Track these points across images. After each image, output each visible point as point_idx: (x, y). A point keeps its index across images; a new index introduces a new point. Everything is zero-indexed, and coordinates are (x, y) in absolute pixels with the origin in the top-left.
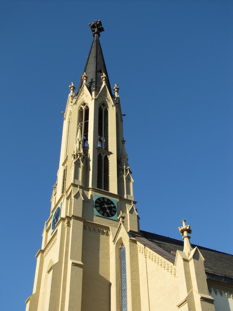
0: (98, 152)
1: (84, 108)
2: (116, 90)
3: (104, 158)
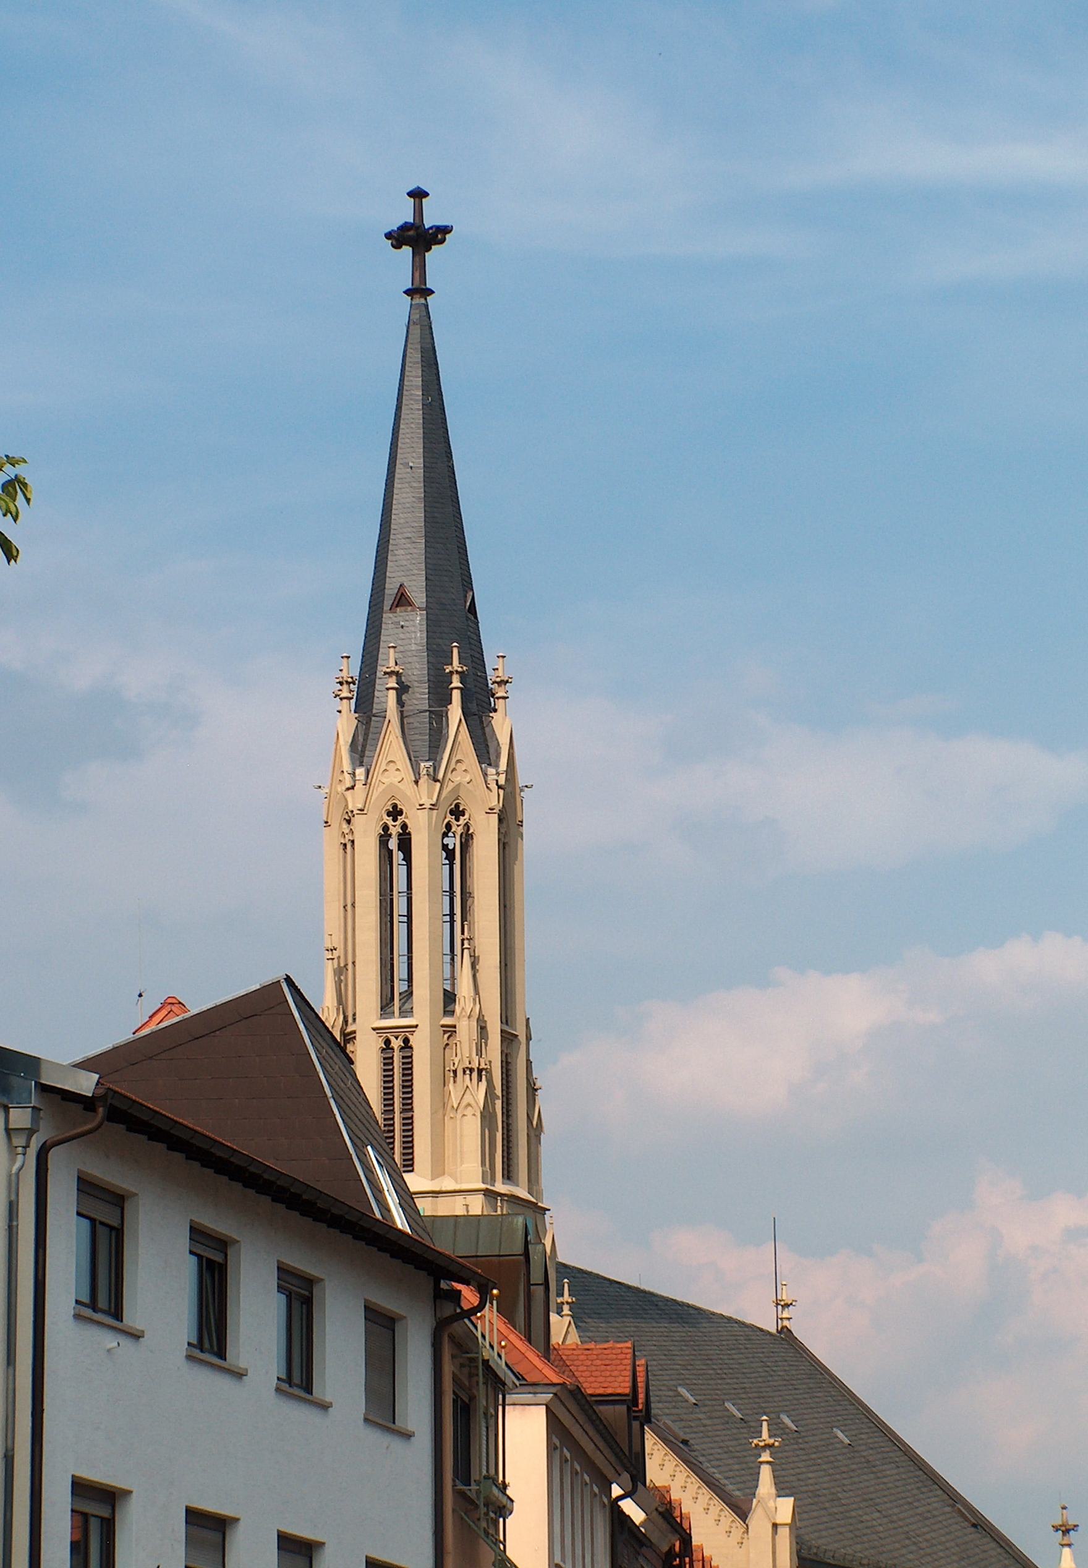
1: (395, 831)
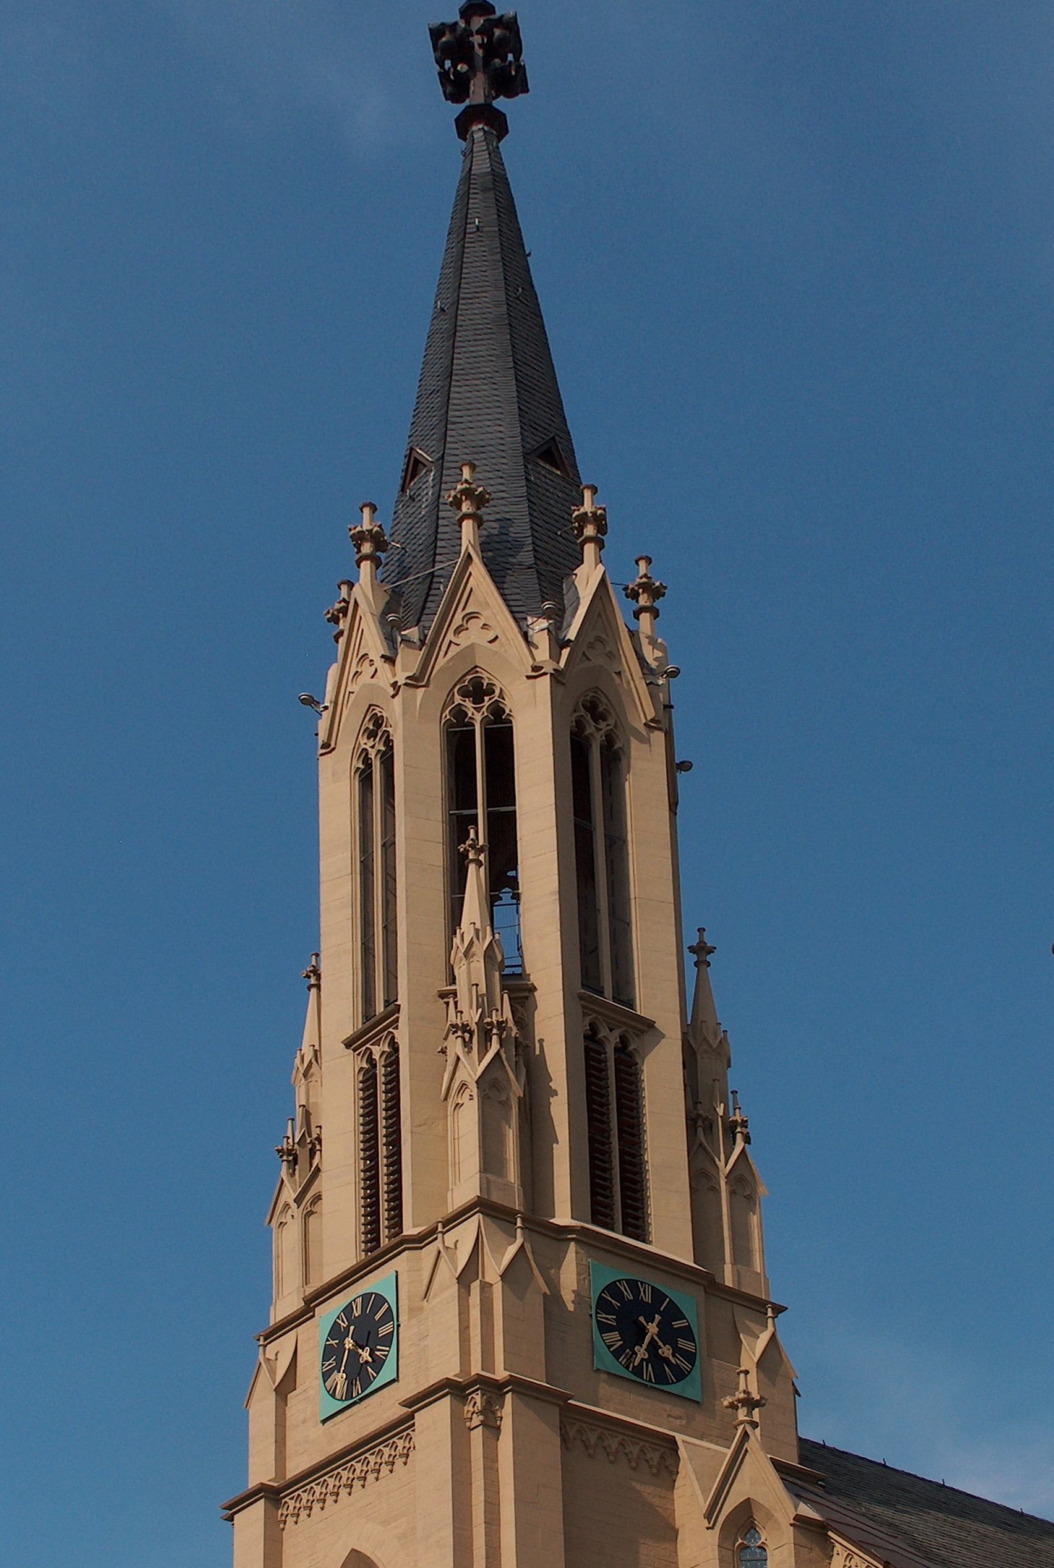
0: (585, 1015)
1: (477, 717)
2: (466, 507)
3: (616, 1050)
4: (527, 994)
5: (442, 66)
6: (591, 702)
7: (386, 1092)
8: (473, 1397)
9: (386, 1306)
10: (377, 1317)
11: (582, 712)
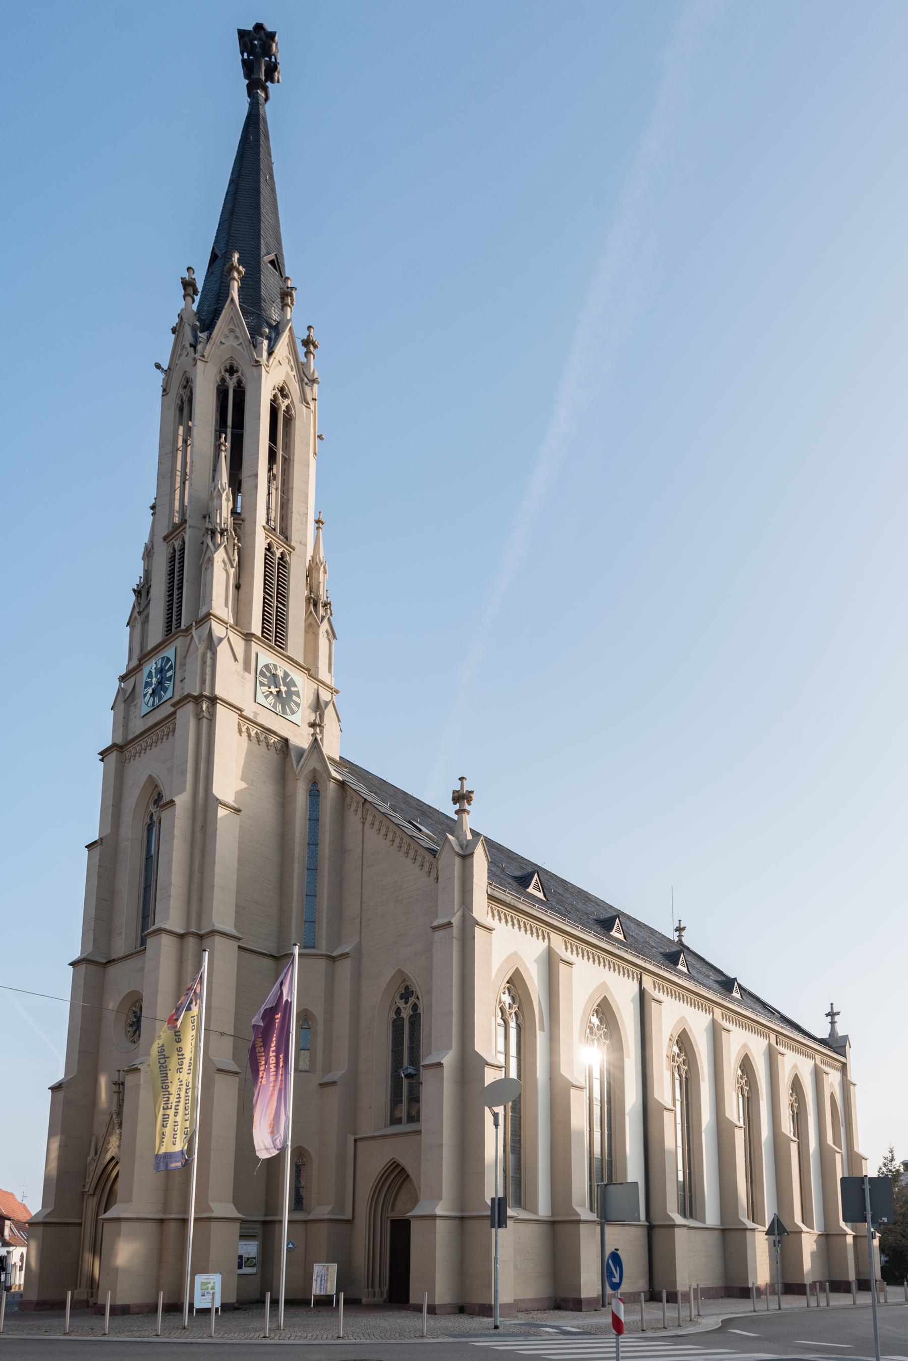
0: (266, 538)
1: (231, 383)
4: (241, 522)
5: (243, 56)
6: (281, 387)
7: (179, 559)
8: (182, 534)
9: (170, 663)
10: (166, 668)
11: (277, 391)
